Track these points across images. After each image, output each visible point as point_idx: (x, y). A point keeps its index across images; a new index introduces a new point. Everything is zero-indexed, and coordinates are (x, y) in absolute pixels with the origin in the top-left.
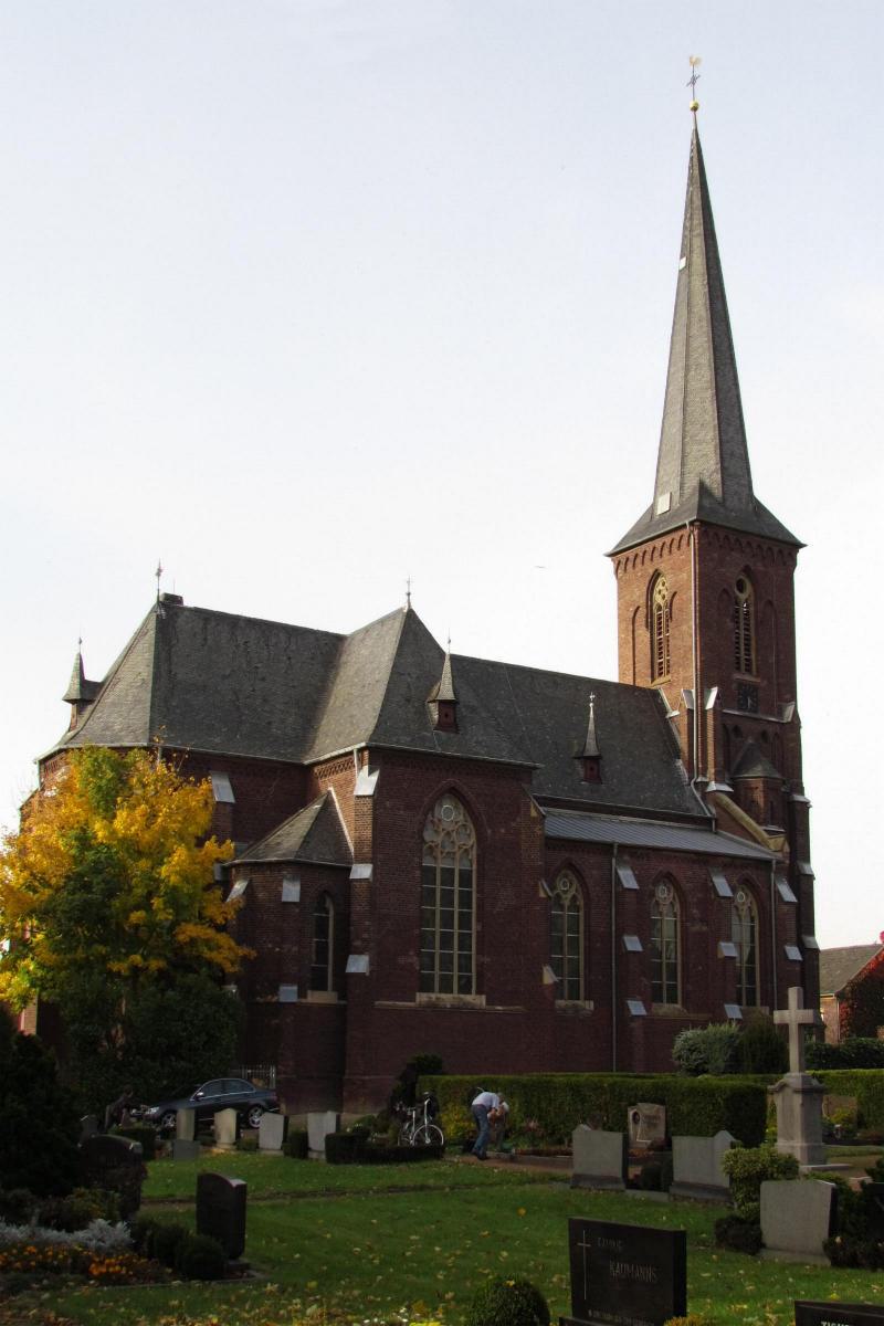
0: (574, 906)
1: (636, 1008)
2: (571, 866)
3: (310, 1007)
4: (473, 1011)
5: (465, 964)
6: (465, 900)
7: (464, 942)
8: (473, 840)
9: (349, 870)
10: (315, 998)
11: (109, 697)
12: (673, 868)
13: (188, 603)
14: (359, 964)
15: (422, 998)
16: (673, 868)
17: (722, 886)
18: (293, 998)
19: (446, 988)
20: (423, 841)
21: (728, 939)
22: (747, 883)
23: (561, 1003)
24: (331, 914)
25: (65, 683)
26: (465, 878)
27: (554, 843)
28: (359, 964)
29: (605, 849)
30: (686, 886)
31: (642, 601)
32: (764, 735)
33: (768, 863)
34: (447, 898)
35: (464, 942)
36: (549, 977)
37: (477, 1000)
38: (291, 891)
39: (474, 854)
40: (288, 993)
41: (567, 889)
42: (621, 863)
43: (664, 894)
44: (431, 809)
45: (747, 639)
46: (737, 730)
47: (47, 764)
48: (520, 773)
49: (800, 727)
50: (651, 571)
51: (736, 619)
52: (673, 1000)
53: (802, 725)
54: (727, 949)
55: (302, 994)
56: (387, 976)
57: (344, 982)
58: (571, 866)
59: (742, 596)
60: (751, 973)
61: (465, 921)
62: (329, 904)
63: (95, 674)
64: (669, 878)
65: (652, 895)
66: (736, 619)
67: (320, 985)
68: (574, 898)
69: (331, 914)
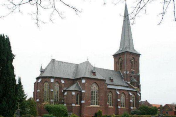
0: (111, 96)
1: (119, 107)
2: (111, 91)
3: (76, 106)
4: (98, 107)
5: (97, 102)
6: (97, 95)
7: (97, 100)
8: (98, 88)
9: (81, 91)
10: (77, 105)
11: (46, 71)
12: (124, 92)
13: (56, 60)
14: (83, 102)
15: (91, 106)
16: (124, 92)
17: (131, 94)
18: (74, 105)
19: (94, 105)
20: (91, 88)
21: (131, 100)
22: (134, 94)
23: (109, 107)
24: (79, 96)
25: (39, 69)
26: (97, 92)
27: (109, 89)
28: (83, 102)
29: (115, 89)
30: (126, 94)
31: (118, 61)
32: (135, 77)
33: (137, 91)
34: (94, 94)
35: (97, 100)
36: (108, 104)
37: (98, 106)
38: (74, 93)
39: (98, 90)
40: (73, 105)
41: (110, 94)
42: (117, 91)
43: (123, 95)
44: (92, 85)
45: (133, 66)
46: (131, 76)
47: (38, 79)
48: (104, 80)
49: (10, 57)
50: (119, 57)
51: (131, 63)
52: (123, 106)
53: (14, 50)
54: (131, 101)
55: (75, 105)
56: (87, 103)
57: (81, 104)
58: (111, 91)
59: (132, 61)
60: (134, 104)
61: (97, 97)
62: (78, 95)
63: (44, 68)
64: (123, 93)
65: (121, 95)
66: (131, 63)
67: (77, 104)
68: (111, 95)
69: (79, 96)
